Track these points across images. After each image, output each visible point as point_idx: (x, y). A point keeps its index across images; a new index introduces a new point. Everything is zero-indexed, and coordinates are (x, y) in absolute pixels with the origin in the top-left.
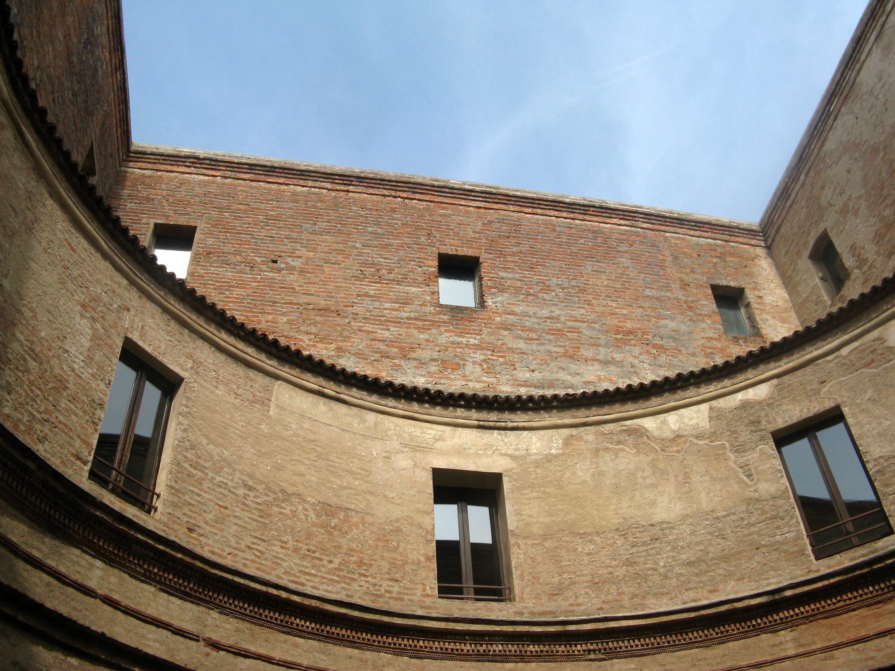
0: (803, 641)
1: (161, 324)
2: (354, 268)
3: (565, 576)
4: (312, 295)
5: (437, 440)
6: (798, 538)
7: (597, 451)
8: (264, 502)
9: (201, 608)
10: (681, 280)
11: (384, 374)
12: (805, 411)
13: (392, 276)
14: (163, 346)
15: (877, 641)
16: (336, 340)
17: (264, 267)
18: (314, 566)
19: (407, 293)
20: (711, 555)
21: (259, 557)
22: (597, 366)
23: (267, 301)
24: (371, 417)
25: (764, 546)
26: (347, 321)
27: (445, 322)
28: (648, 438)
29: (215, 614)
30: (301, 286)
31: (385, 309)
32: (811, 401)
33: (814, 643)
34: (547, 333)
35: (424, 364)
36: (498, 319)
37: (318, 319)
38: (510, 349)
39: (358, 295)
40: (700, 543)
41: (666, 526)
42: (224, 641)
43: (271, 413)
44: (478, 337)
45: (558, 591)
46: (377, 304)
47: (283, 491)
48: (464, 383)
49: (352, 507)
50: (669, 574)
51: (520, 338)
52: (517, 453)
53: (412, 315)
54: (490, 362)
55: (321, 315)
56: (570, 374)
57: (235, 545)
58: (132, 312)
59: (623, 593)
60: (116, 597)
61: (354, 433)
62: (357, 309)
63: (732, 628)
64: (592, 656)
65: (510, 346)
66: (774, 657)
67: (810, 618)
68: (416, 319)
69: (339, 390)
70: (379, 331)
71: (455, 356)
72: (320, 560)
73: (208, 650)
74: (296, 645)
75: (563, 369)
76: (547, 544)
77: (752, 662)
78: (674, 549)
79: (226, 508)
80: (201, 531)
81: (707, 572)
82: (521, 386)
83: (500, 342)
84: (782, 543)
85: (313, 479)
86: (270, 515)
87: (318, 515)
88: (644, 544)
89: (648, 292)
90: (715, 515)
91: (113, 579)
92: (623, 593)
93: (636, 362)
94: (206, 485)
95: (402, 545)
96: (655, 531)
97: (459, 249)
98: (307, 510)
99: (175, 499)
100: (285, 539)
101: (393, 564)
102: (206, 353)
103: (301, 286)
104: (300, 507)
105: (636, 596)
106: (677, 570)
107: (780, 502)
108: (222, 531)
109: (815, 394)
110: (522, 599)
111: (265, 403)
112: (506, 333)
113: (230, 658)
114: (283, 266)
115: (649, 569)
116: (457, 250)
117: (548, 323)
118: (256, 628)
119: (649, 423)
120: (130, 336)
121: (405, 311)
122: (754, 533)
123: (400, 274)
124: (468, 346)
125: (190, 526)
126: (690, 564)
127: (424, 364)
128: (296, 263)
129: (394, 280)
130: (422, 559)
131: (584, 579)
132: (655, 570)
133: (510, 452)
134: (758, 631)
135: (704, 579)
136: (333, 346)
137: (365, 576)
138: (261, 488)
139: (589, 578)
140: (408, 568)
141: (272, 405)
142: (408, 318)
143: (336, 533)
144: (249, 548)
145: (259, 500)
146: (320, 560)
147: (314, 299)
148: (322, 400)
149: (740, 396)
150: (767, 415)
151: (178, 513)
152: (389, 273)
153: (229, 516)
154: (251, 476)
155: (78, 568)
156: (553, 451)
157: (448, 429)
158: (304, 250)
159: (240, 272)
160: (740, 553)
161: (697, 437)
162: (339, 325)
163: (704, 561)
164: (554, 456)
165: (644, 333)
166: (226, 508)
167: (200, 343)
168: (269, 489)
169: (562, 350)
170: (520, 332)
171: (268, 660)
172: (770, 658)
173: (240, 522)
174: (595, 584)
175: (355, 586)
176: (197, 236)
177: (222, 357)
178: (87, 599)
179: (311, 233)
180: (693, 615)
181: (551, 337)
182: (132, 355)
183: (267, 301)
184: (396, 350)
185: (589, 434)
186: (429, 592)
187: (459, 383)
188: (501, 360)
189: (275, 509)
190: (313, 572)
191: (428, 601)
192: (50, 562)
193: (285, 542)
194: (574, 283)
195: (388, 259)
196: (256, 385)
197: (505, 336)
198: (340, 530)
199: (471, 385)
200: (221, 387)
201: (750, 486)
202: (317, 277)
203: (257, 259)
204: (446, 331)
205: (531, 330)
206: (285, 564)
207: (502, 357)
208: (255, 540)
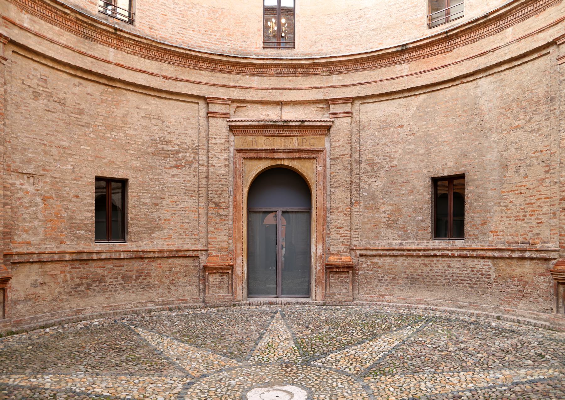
0: (411, 69)
3: (318, 36)
6: (422, 18)
9: (160, 63)
20: (383, 26)
21: (183, 37)
29: (165, 65)
42: (170, 76)
50: (363, 35)
57: (171, 33)
59: (342, 44)
60: (122, 63)
63: (384, 62)
66: (398, 76)
72: (211, 35)
78: (368, 21)
79: (166, 15)
80: (156, 28)
81: (380, 34)
86: (187, 16)
91: (119, 56)
92: (342, 44)
98: (204, 11)
99: (142, 15)
100: (194, 27)
105: (347, 46)
108: (165, 27)
113: (174, 82)
115: (355, 32)
125: (150, 27)
126: (374, 30)
130: (256, 31)
132: (357, 33)
137: (231, 41)
139: (329, 37)
143: (217, 21)
144: (178, 33)
146: (211, 35)
151: (144, 21)
153: (167, 19)
155: (103, 53)
160: (395, 25)
163: (379, 29)
166: (166, 15)
171: (189, 81)
172: (396, 76)
173: (173, 21)
174: (331, 40)
175: (226, 45)
180: (368, 55)
186: (258, 46)
189: (189, 13)
190: (207, 41)
192: (90, 53)
193: (194, 28)
198: (219, 20)
208: (181, 29)
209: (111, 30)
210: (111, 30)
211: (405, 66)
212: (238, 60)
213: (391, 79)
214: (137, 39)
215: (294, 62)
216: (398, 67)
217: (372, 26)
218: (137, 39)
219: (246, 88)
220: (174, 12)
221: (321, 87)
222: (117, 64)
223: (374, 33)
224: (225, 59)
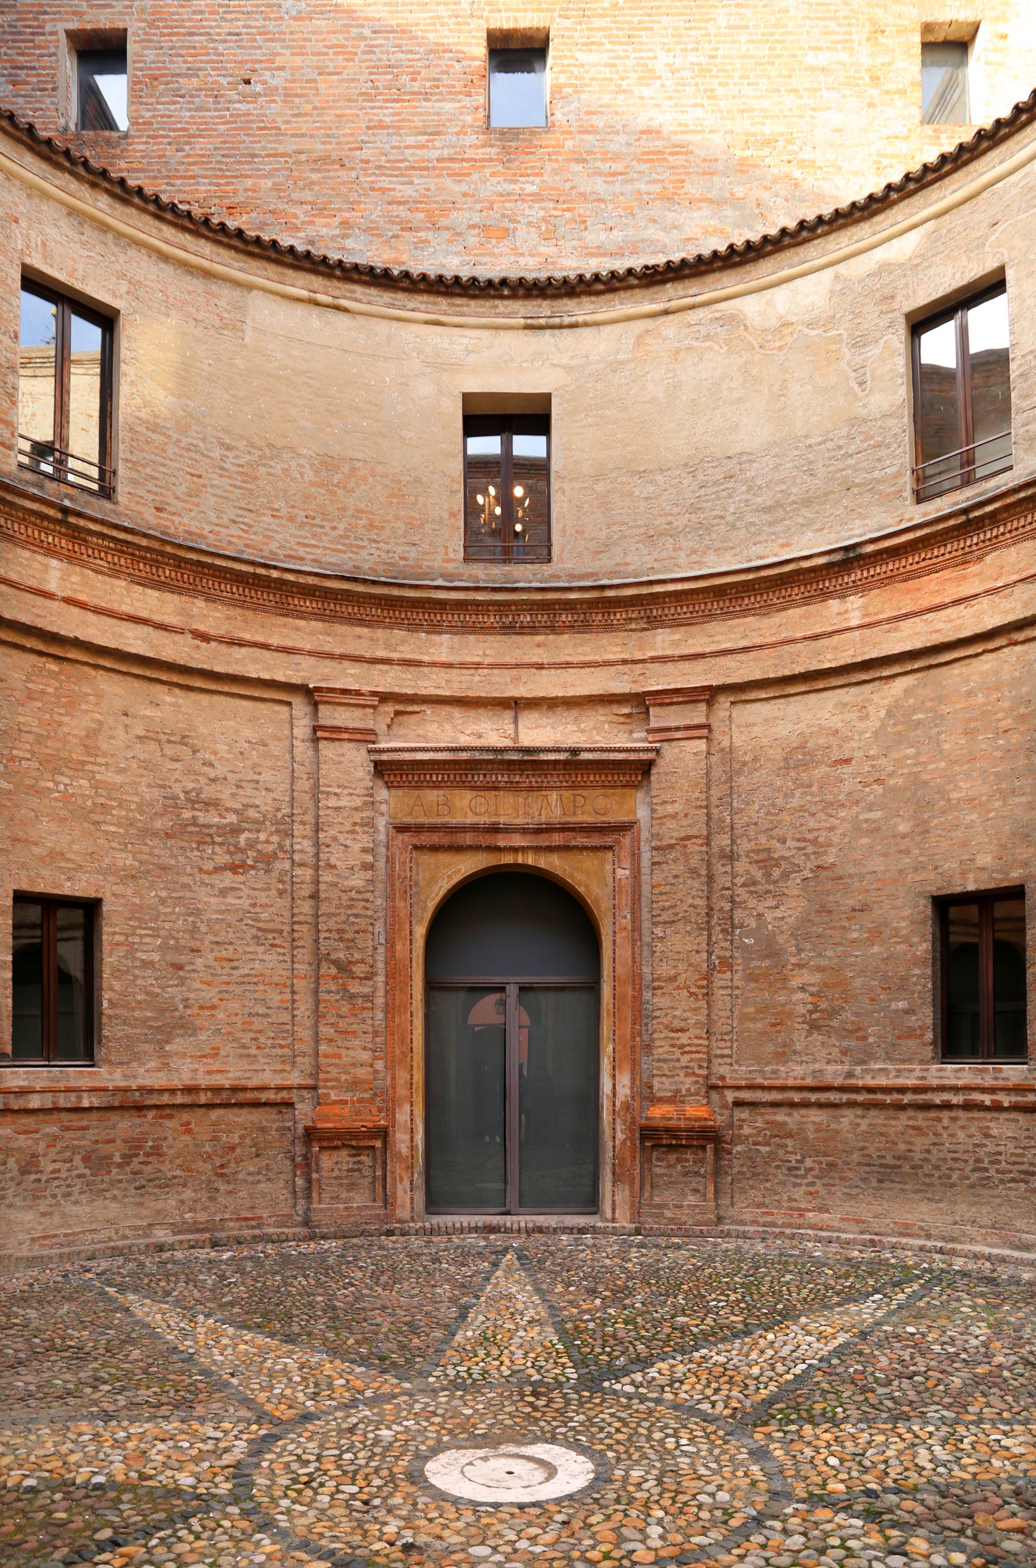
0: (871, 610)
1: (71, 233)
2: (362, 78)
3: (615, 528)
4: (303, 135)
5: (469, 352)
6: (898, 475)
7: (677, 352)
8: (248, 463)
9: (184, 598)
10: (873, 22)
11: (405, 257)
12: (958, 276)
13: (416, 86)
14: (80, 267)
15: (950, 610)
16: (340, 210)
17: (233, 95)
18: (314, 535)
19: (438, 114)
20: (793, 498)
22: (706, 210)
23: (243, 155)
24: (383, 327)
25: (859, 485)
26: (354, 174)
27: (491, 160)
28: (746, 329)
30: (288, 122)
31: (407, 147)
32: (969, 259)
33: (881, 612)
34: (639, 161)
35: (460, 234)
36: (569, 144)
37: (315, 176)
38: (584, 196)
39: (368, 128)
40: (783, 481)
41: (745, 458)
42: (213, 632)
43: (247, 340)
44: (538, 179)
45: (606, 546)
46: (395, 141)
47: (271, 446)
48: (513, 259)
49: (360, 456)
51: (599, 173)
52: (574, 362)
53: (446, 153)
54: (552, 220)
55: (318, 171)
56: (664, 229)
58: (23, 223)
60: (82, 597)
61: (360, 355)
62: (366, 153)
64: (633, 626)
65: (582, 189)
67: (889, 580)
68: (451, 160)
69: (337, 293)
70: (399, 187)
71: (503, 216)
73: (197, 642)
74: (297, 629)
75: (654, 221)
76: (599, 487)
77: (809, 633)
78: (750, 488)
82: (591, 255)
83: (568, 185)
84: (878, 481)
85: (308, 424)
86: (256, 478)
87: (317, 472)
88: (716, 483)
89: (811, 59)
90: (808, 442)
93: (765, 195)
94: (171, 450)
95: (421, 499)
96: (731, 465)
97: (519, 15)
99: (135, 475)
101: (410, 524)
102: (145, 268)
103: (288, 122)
104: (293, 464)
106: (749, 518)
107: (891, 422)
109: (978, 247)
110: (561, 560)
111: (237, 327)
112: (578, 168)
113: (224, 648)
114: (259, 88)
116: (516, 20)
117: (642, 142)
118: (250, 614)
119: (750, 307)
120: (28, 261)
121: (435, 148)
122: (849, 467)
123: (428, 80)
124: (521, 197)
126: (767, 510)
127: (460, 234)
128: (278, 80)
129: (419, 93)
130: (445, 515)
131: (637, 531)
133: (564, 361)
134: (825, 595)
135: (778, 528)
136: (337, 220)
138: (242, 445)
139: (643, 530)
140: (428, 528)
141: (248, 329)
142: (439, 160)
143: (340, 492)
145: (241, 461)
147: (305, 144)
148: (317, 310)
149: (879, 255)
150: (907, 285)
151: (141, 491)
152: (413, 80)
154: (227, 432)
156: (621, 357)
157: (485, 334)
158: (287, 52)
159: (200, 109)
160: (826, 494)
161: (809, 325)
162: (343, 183)
164: (622, 363)
165: (789, 142)
167: (132, 252)
168: (252, 445)
169: (657, 188)
170: (599, 164)
171: (265, 647)
172: (829, 629)
173: (219, 492)
174: (650, 538)
175: (364, 553)
176: (131, 48)
177: (169, 270)
178: (48, 602)
179: (295, 19)
181: (644, 167)
182: (34, 283)
183: (243, 155)
184: (421, 215)
185: (669, 327)
186: (451, 555)
187: (504, 260)
188: (567, 214)
189: (262, 470)
191: (450, 567)
194: (692, 58)
195: (411, 52)
196: (222, 303)
197: (575, 173)
199: (522, 261)
200: (173, 313)
201: (859, 400)
202: (308, 102)
203: (221, 79)
204: (493, 175)
205: (616, 157)
206: (278, 537)
207: (568, 210)
209: (52, 512)
210: (52, 512)
211: (855, 602)
212: (396, 592)
213: (816, 637)
214: (122, 536)
215: (550, 596)
216: (834, 604)
217: (760, 500)
218: (122, 536)
219: (418, 664)
220: (222, 468)
221: (625, 662)
222: (69, 601)
223: (768, 517)
224: (360, 588)
